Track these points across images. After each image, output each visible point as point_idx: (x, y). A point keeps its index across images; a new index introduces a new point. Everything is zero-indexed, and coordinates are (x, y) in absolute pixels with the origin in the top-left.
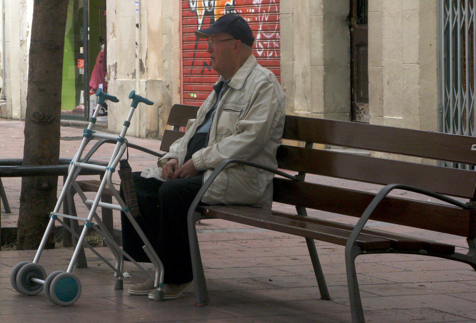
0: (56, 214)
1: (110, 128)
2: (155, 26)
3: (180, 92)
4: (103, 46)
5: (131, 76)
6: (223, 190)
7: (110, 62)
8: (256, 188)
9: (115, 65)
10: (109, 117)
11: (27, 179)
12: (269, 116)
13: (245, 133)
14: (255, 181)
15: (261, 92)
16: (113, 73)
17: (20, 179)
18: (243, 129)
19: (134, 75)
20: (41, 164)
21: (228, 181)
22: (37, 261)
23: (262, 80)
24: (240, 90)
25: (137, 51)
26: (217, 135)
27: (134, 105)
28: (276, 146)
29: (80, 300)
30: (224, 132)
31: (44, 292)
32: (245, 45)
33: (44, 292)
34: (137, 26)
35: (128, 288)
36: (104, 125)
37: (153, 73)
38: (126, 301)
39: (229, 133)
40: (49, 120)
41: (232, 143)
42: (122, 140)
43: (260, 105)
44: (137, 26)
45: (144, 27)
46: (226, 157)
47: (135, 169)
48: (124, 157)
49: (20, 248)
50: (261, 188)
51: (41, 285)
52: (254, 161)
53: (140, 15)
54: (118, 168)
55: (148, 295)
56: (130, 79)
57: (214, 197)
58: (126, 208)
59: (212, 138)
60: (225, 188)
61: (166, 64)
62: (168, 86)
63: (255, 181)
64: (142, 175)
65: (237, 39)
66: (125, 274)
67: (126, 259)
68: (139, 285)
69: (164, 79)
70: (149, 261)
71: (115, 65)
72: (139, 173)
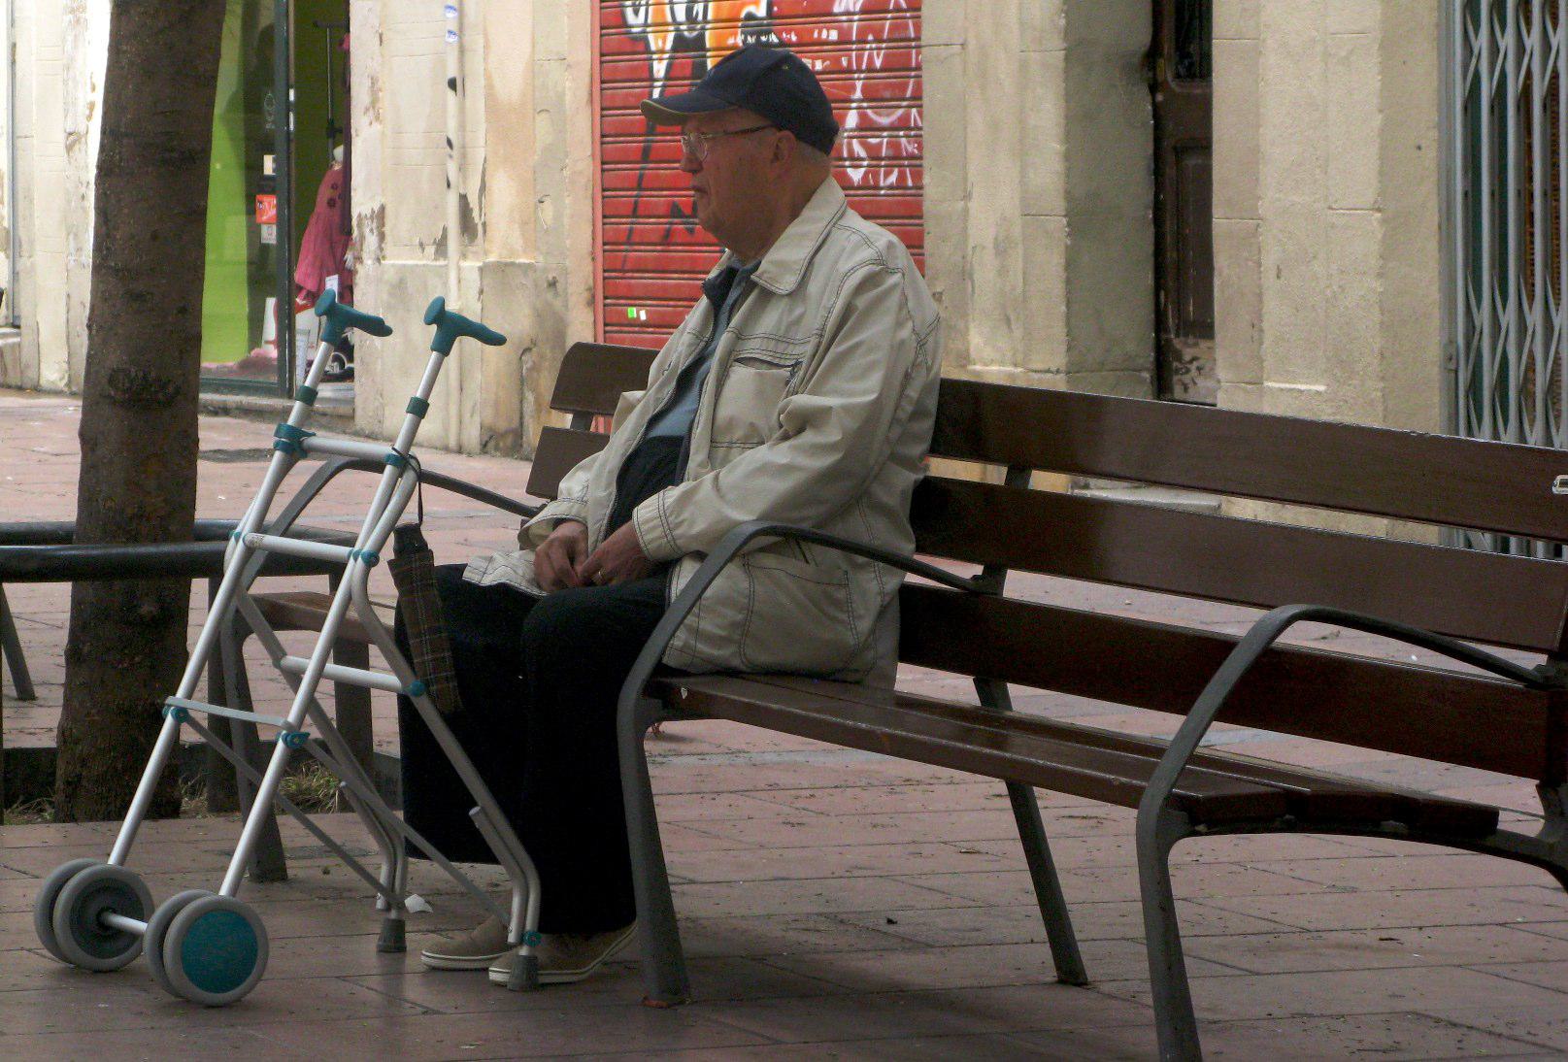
0: (187, 704)
1: (361, 421)
2: (511, 85)
3: (592, 302)
4: (339, 152)
5: (431, 250)
6: (734, 625)
7: (362, 204)
8: (844, 617)
9: (380, 215)
10: (360, 386)
11: (90, 589)
12: (887, 381)
13: (808, 437)
14: (841, 594)
15: (861, 302)
16: (371, 240)
17: (66, 588)
18: (801, 423)
19: (441, 246)
20: (134, 538)
21: (751, 596)
22: (123, 858)
23: (862, 264)
24: (791, 295)
25: (452, 168)
26: (713, 442)
27: (443, 347)
28: (907, 479)
29: (265, 988)
30: (739, 433)
31: (145, 960)
32: (808, 150)
33: (145, 960)
34: (452, 84)
35: (423, 950)
36: (343, 409)
37: (504, 239)
38: (415, 990)
39: (754, 438)
40: (160, 396)
41: (764, 469)
42: (403, 461)
43: (857, 345)
44: (452, 84)
45: (475, 88)
46: (745, 515)
47: (443, 555)
48: (410, 516)
49: (67, 816)
50: (860, 617)
51: (134, 937)
52: (838, 531)
53: (462, 50)
54: (388, 553)
55: (486, 970)
56: (427, 259)
57: (704, 648)
58: (413, 683)
59: (697, 455)
60: (740, 617)
61: (547, 212)
62: (553, 284)
63: (841, 594)
64: (467, 575)
65: (780, 128)
66: (413, 902)
67: (414, 851)
68: (460, 937)
69: (540, 260)
70: (490, 858)
71: (380, 215)
72: (459, 569)
